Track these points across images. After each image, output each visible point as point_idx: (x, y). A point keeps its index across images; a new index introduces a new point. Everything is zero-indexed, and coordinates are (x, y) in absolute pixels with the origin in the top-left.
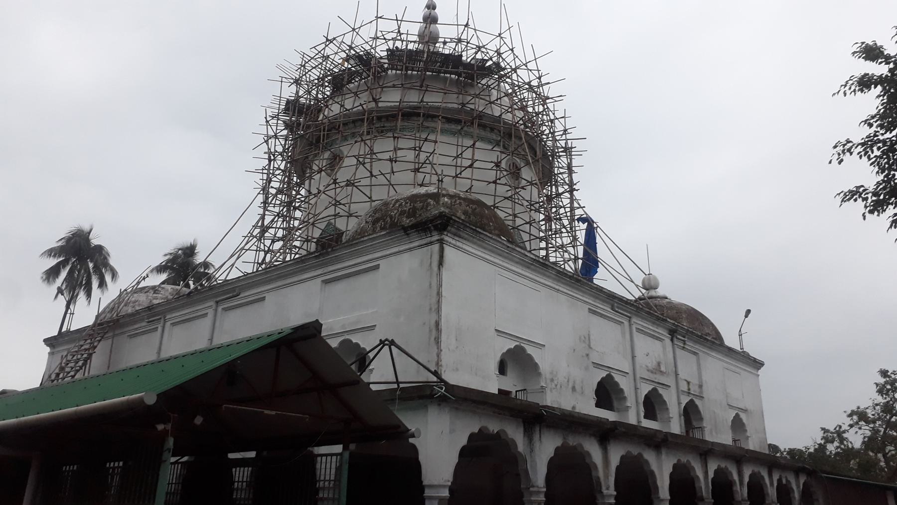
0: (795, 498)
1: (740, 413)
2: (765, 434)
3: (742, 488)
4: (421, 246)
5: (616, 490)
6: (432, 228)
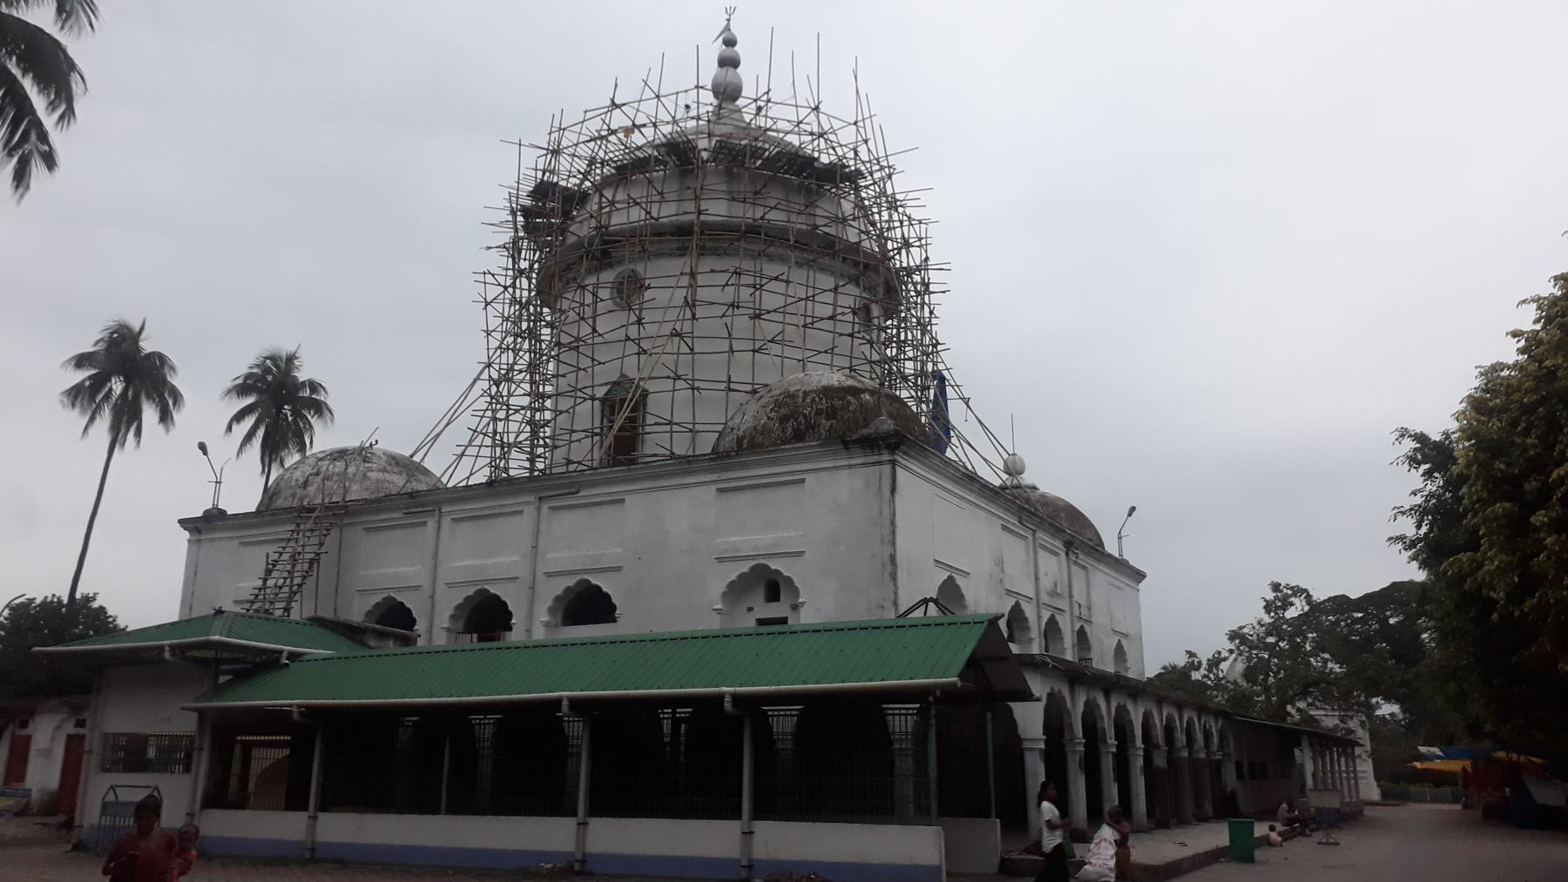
0: (1213, 743)
1: (1084, 625)
4: (865, 465)
5: (1143, 743)
6: (883, 446)
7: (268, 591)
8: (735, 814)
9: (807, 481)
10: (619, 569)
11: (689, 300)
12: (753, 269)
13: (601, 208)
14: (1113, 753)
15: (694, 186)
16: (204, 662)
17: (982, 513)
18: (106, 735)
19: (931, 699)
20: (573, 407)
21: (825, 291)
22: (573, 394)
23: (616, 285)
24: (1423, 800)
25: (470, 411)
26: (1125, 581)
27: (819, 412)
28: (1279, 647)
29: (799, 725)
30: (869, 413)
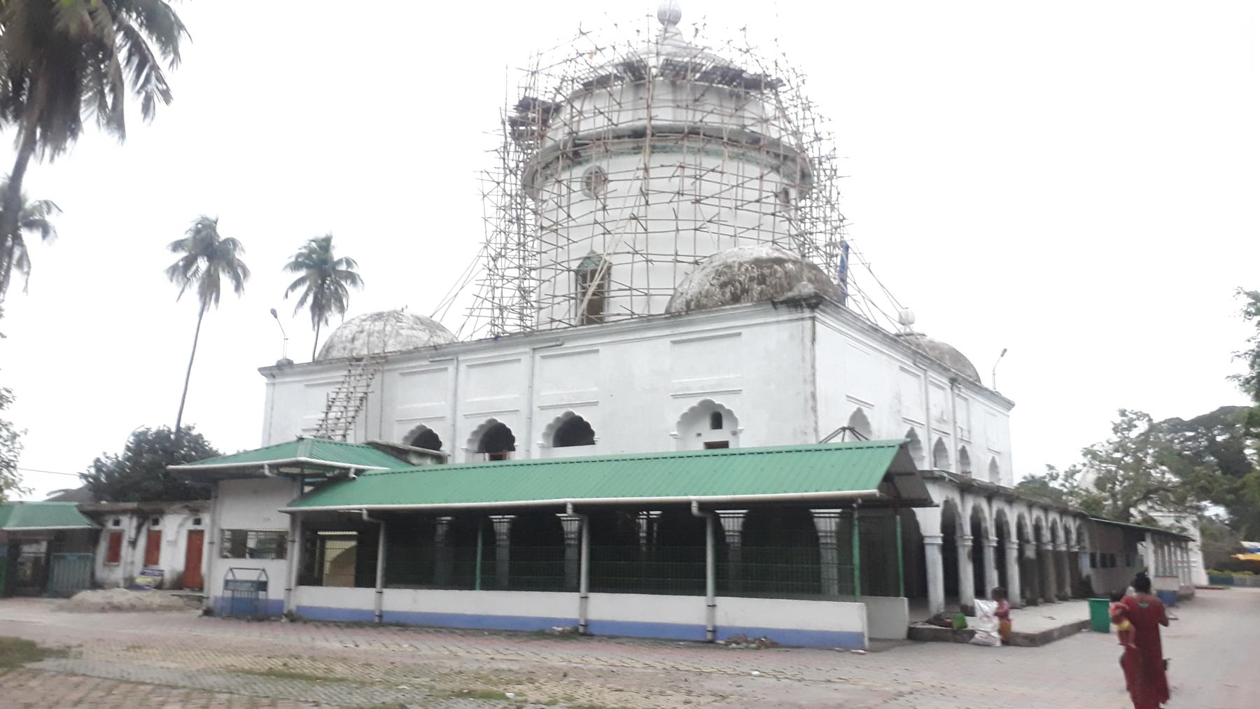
1: (995, 456)
2: (1012, 474)
7: (330, 422)
8: (700, 590)
9: (743, 335)
10: (595, 404)
11: (643, 190)
12: (693, 163)
13: (572, 117)
14: (994, 547)
15: (647, 96)
16: (293, 477)
17: (884, 357)
18: (222, 531)
19: (855, 505)
20: (555, 277)
21: (753, 179)
22: (554, 267)
23: (585, 179)
24: (1243, 584)
25: (473, 282)
26: (981, 400)
27: (751, 279)
28: (1124, 461)
29: (744, 525)
30: (791, 279)
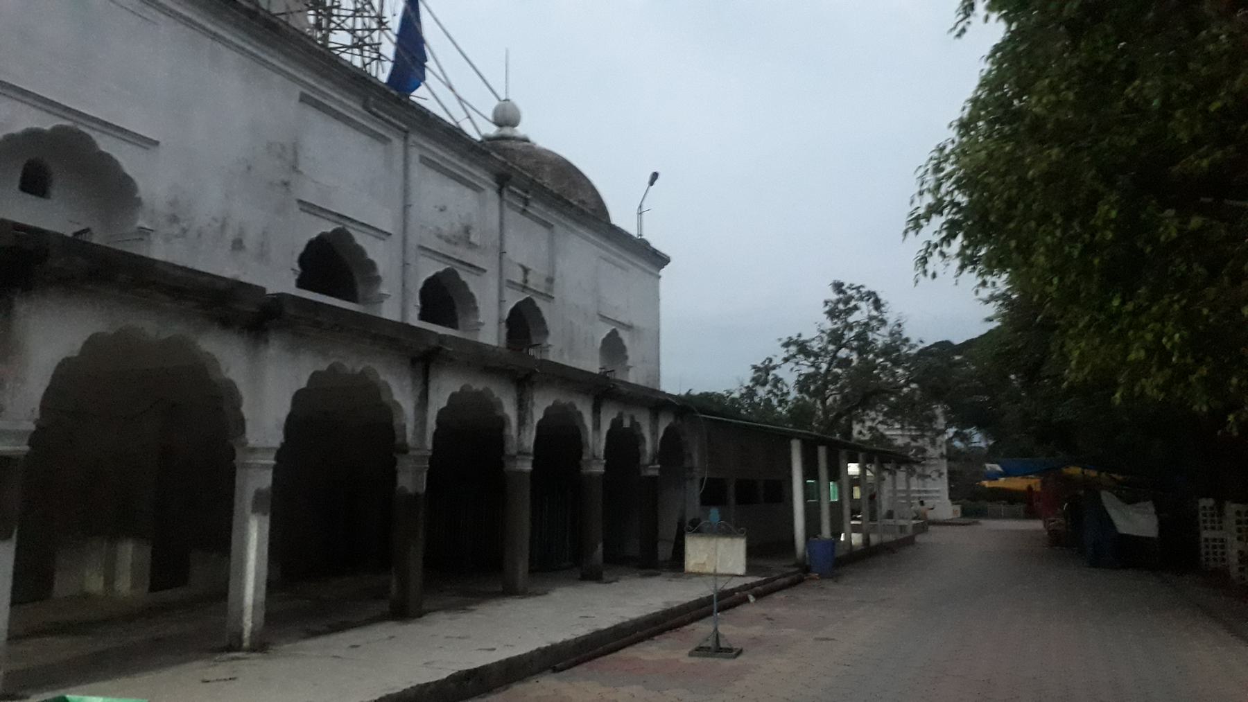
0: (645, 451)
1: (618, 329)
2: (658, 364)
3: (522, 431)
17: (277, 78)
24: (997, 516)
